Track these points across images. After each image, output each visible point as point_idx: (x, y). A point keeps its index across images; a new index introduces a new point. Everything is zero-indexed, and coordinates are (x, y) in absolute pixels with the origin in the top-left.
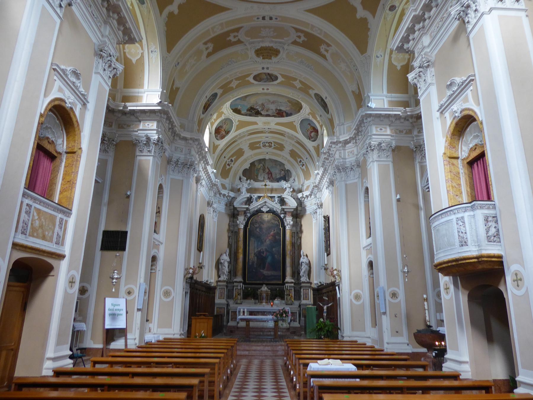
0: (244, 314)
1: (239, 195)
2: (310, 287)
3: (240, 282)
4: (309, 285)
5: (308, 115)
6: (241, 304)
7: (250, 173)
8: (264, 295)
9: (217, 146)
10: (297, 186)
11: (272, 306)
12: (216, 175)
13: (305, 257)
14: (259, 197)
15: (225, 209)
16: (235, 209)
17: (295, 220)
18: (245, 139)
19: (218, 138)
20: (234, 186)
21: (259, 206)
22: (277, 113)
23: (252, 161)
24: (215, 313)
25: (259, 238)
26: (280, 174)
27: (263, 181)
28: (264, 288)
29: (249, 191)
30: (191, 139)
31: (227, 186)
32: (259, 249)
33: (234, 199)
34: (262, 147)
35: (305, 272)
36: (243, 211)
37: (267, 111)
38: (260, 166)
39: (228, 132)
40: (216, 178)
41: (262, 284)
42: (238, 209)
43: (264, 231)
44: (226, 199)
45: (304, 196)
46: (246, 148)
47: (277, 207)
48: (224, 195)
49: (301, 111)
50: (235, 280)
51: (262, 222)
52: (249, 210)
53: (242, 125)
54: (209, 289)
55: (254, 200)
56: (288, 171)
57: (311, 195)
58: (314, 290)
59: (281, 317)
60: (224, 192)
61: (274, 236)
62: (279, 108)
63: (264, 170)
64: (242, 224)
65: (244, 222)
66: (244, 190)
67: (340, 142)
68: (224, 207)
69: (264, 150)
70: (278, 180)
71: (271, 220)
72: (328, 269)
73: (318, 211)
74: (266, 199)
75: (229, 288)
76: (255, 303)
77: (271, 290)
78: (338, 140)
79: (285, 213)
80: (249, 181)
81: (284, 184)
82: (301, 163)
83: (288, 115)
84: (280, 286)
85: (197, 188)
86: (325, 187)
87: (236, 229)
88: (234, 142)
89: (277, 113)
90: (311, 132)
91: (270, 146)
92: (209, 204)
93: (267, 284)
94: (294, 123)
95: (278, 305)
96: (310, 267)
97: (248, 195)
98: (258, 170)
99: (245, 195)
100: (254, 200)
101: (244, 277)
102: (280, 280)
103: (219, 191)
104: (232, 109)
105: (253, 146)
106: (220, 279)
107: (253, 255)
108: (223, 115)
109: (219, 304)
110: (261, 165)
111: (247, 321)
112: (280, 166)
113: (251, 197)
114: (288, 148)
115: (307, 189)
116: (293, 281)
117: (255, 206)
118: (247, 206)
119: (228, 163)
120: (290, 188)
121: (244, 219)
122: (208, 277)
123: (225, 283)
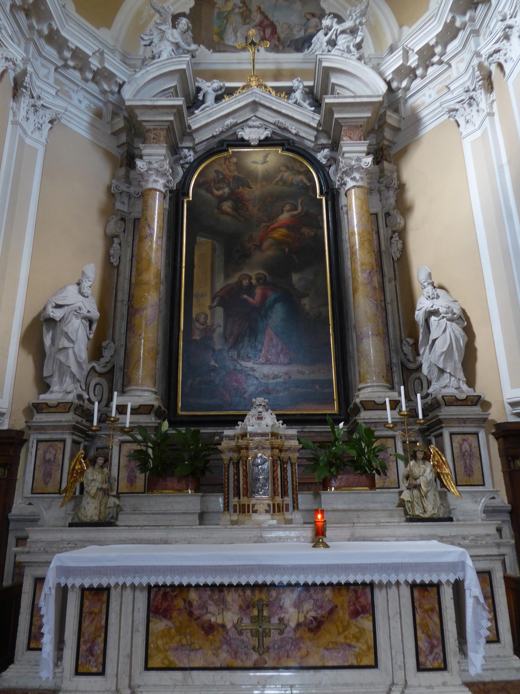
2: (483, 421)
4: (476, 411)
6: (107, 522)
8: (262, 460)
21: (229, 121)
51: (244, 178)
61: (293, 226)
76: (203, 517)
98: (225, 17)
106: (44, 397)
107: (207, 301)
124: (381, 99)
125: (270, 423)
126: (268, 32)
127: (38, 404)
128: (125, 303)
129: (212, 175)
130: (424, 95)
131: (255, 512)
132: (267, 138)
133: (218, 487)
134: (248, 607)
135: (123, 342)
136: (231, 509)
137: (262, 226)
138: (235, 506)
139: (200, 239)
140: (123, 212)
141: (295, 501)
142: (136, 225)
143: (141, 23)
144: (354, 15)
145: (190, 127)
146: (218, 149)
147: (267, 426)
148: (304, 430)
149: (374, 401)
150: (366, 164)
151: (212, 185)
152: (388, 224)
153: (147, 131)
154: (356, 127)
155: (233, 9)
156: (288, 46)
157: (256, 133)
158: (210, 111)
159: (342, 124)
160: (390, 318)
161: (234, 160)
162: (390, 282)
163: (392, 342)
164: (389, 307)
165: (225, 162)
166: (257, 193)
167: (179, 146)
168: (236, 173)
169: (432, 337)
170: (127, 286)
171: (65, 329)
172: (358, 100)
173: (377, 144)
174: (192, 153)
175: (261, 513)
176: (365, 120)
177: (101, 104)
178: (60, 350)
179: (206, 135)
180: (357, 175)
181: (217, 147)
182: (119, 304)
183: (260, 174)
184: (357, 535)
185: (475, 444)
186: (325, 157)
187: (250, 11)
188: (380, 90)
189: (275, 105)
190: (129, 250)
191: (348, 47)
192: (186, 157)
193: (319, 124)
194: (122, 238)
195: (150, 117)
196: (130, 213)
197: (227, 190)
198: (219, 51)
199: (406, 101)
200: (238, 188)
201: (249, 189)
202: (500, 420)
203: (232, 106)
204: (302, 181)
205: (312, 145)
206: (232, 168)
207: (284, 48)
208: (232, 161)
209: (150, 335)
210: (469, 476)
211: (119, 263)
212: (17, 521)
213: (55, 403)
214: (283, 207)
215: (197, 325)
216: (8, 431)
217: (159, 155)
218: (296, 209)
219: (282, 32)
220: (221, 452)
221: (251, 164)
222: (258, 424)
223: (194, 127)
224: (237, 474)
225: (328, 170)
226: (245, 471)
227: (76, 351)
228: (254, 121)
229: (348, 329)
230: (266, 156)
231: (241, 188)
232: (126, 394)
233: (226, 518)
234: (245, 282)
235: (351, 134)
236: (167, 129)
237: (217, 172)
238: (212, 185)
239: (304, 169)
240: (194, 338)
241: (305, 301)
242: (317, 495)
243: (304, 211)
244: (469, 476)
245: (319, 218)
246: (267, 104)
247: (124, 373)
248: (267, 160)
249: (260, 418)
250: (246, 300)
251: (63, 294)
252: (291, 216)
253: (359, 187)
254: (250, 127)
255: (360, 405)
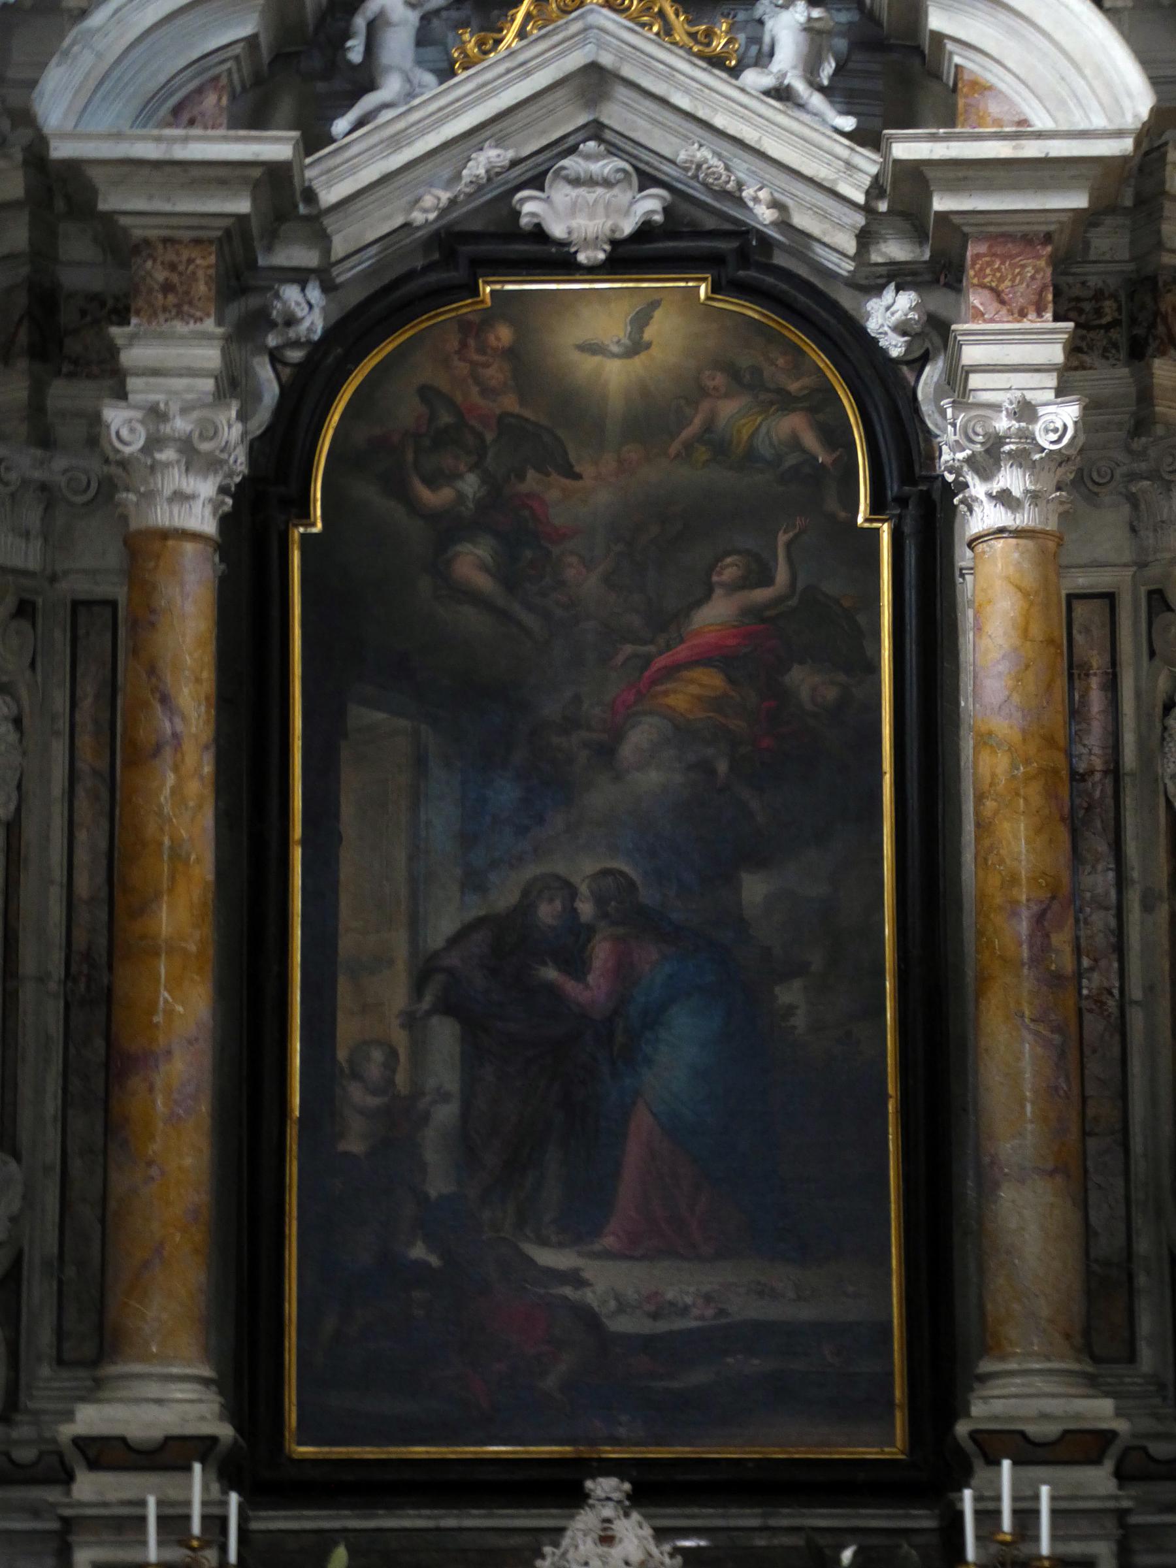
3: (169, 1455)
17: (1114, 377)
21: (484, 161)
32: (504, 896)
41: (563, 1488)
42: (110, 201)
43: (584, 579)
47: (792, 150)
50: (91, 1419)
51: (546, 426)
55: (398, 44)
61: (755, 657)
64: (193, 457)
65: (231, 432)
71: (695, 392)
79: (941, 270)
87: (92, 566)
100: (398, 44)
101: (247, 1371)
107: (395, 992)
116: (1100, 1411)
118: (276, 147)
121: (233, 384)
124: (1126, 146)
128: (53, 986)
129: (407, 412)
132: (645, 231)
135: (52, 1155)
137: (620, 658)
140: (25, 573)
142: (81, 632)
145: (310, 196)
146: (433, 278)
147: (627, 1563)
148: (772, 1522)
149: (1022, 1434)
150: (1054, 437)
151: (410, 457)
152: (1157, 646)
154: (1027, 240)
157: (601, 210)
158: (401, 125)
159: (966, 229)
160: (1136, 1065)
161: (504, 334)
162: (1148, 907)
163: (1140, 1167)
165: (464, 345)
166: (603, 497)
167: (262, 262)
168: (510, 403)
170: (56, 912)
172: (1032, 149)
173: (1133, 259)
174: (314, 293)
176: (1070, 214)
179: (378, 223)
180: (1012, 479)
181: (428, 268)
183: (616, 405)
186: (901, 329)
188: (1126, 103)
189: (687, 91)
190: (59, 749)
192: (291, 321)
194: (24, 693)
195: (151, 197)
196: (53, 579)
200: (521, 477)
201: (567, 482)
203: (494, 92)
206: (495, 373)
208: (492, 339)
209: (188, 1161)
211: (18, 809)
214: (711, 569)
215: (356, 1093)
217: (192, 373)
218: (766, 579)
221: (576, 356)
222: (600, 1556)
223: (329, 196)
225: (911, 378)
228: (588, 157)
229: (965, 1110)
230: (641, 320)
231: (531, 474)
232: (106, 1394)
234: (547, 912)
235: (1001, 280)
236: (220, 239)
237: (427, 393)
238: (410, 457)
239: (806, 381)
240: (343, 1146)
243: (800, 586)
245: (861, 619)
246: (647, 82)
247: (60, 1283)
248: (648, 334)
249: (607, 1539)
250: (551, 989)
253: (1018, 533)
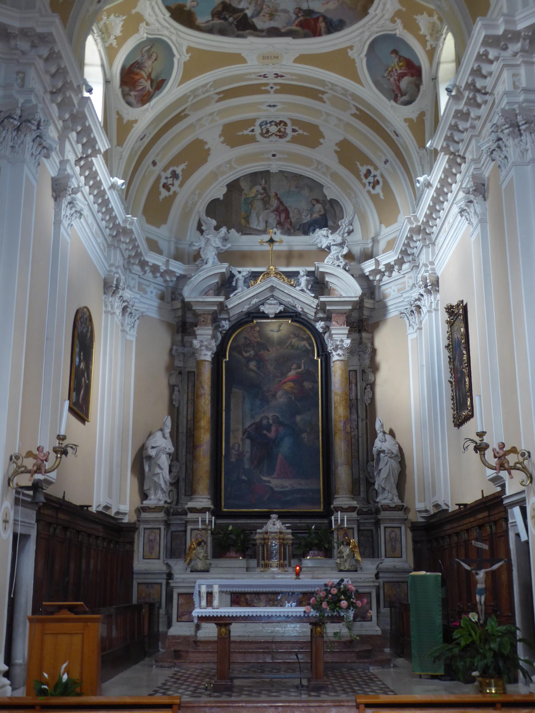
0: (210, 603)
1: (198, 269)
3: (203, 511)
4: (399, 514)
5: (393, 21)
7: (228, 210)
8: (275, 544)
9: (131, 124)
10: (358, 242)
11: (298, 574)
12: (126, 195)
13: (388, 437)
14: (255, 276)
15: (160, 308)
16: (186, 306)
17: (356, 336)
18: (209, 109)
19: (132, 99)
20: (184, 246)
22: (301, 24)
23: (230, 177)
24: (135, 601)
25: (256, 391)
26: (311, 212)
27: (264, 232)
28: (275, 525)
29: (223, 256)
30: (24, 33)
31: (163, 245)
32: (257, 419)
33: (183, 279)
34: (259, 138)
35: (387, 478)
36: (208, 313)
37: (272, 16)
38: (254, 190)
39: (159, 85)
40: (112, 175)
41: (267, 516)
43: (271, 368)
44: (160, 280)
45: (382, 268)
46: (212, 138)
47: (305, 300)
48: (155, 269)
49: (371, 11)
50: (190, 505)
51: (264, 344)
52: (227, 311)
53: (200, 61)
54: (114, 533)
56: (334, 203)
57: (400, 262)
58: (415, 527)
59: (333, 610)
60: (152, 258)
61: (299, 380)
62: (305, 6)
63: (266, 202)
64: (208, 349)
65: (214, 345)
66: (210, 255)
67: (515, 36)
68: (156, 303)
69: (265, 145)
70: (307, 229)
72: (487, 446)
73: (426, 302)
74: (275, 281)
75: (173, 529)
76: (248, 569)
77: (295, 530)
78: (511, 28)
79: (328, 319)
80: (224, 230)
81: (322, 237)
82: (371, 179)
83: (334, 26)
84: (318, 521)
85: (57, 214)
86: (455, 210)
87: (191, 366)
88: (178, 118)
89: (301, 24)
90: (401, 76)
91: (282, 135)
92: (110, 287)
93: (282, 516)
94: (350, 53)
95: (318, 574)
96: (402, 463)
97: (223, 268)
98: (250, 202)
99: (213, 268)
100: (241, 283)
101: (216, 498)
102: (316, 502)
103: (138, 255)
104: (168, 8)
105: (234, 134)
107: (240, 435)
108: (143, 25)
109: (146, 573)
110: (259, 188)
111: (219, 625)
112: (311, 189)
113: (232, 276)
114: (332, 136)
115: (390, 245)
116: (354, 503)
117: (241, 300)
118: (221, 299)
119: (163, 181)
120: (341, 245)
121: (214, 337)
122: (110, 496)
123: (161, 515)
124: (357, 299)
125: (279, 527)
126: (283, 216)
127: (144, 507)
128: (184, 434)
129: (242, 341)
130: (391, 287)
131: (271, 567)
132: (280, 312)
133: (254, 556)
134: (269, 601)
136: (260, 566)
138: (262, 565)
139: (235, 390)
141: (290, 563)
143: (187, 211)
144: (344, 225)
145: (226, 307)
146: (246, 320)
153: (199, 315)
154: (342, 314)
155: (256, 196)
156: (298, 230)
160: (360, 446)
161: (257, 329)
162: (362, 421)
163: (361, 463)
164: (360, 439)
168: (259, 339)
169: (380, 468)
171: (158, 462)
172: (342, 299)
174: (227, 322)
175: (274, 568)
177: (163, 288)
178: (155, 474)
182: (180, 435)
184: (315, 577)
185: (398, 533)
186: (322, 328)
187: (269, 196)
190: (186, 396)
191: (337, 256)
192: (223, 326)
193: (317, 306)
194: (180, 386)
196: (185, 368)
197: (252, 353)
198: (246, 234)
199: (380, 287)
202: (414, 520)
204: (305, 346)
205: (313, 318)
206: (256, 335)
207: (294, 231)
210: (394, 552)
212: (138, 574)
213: (154, 506)
216: (127, 523)
218: (300, 368)
219: (294, 217)
220: (255, 540)
223: (229, 307)
224: (263, 550)
226: (267, 549)
227: (164, 475)
231: (262, 351)
233: (258, 570)
234: (265, 422)
237: (245, 338)
241: (304, 435)
242: (300, 561)
244: (394, 552)
249: (274, 525)
250: (265, 435)
251: (154, 439)
252: (297, 373)
253: (341, 360)
254: (269, 304)
255: (333, 509)
